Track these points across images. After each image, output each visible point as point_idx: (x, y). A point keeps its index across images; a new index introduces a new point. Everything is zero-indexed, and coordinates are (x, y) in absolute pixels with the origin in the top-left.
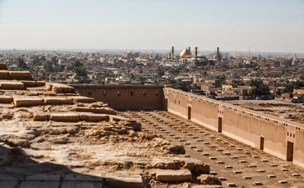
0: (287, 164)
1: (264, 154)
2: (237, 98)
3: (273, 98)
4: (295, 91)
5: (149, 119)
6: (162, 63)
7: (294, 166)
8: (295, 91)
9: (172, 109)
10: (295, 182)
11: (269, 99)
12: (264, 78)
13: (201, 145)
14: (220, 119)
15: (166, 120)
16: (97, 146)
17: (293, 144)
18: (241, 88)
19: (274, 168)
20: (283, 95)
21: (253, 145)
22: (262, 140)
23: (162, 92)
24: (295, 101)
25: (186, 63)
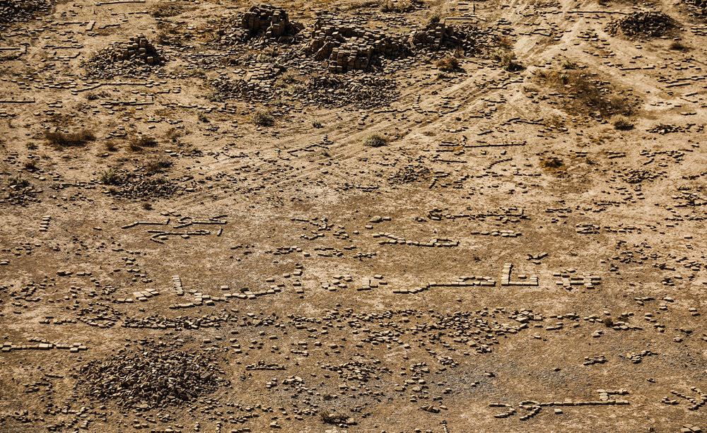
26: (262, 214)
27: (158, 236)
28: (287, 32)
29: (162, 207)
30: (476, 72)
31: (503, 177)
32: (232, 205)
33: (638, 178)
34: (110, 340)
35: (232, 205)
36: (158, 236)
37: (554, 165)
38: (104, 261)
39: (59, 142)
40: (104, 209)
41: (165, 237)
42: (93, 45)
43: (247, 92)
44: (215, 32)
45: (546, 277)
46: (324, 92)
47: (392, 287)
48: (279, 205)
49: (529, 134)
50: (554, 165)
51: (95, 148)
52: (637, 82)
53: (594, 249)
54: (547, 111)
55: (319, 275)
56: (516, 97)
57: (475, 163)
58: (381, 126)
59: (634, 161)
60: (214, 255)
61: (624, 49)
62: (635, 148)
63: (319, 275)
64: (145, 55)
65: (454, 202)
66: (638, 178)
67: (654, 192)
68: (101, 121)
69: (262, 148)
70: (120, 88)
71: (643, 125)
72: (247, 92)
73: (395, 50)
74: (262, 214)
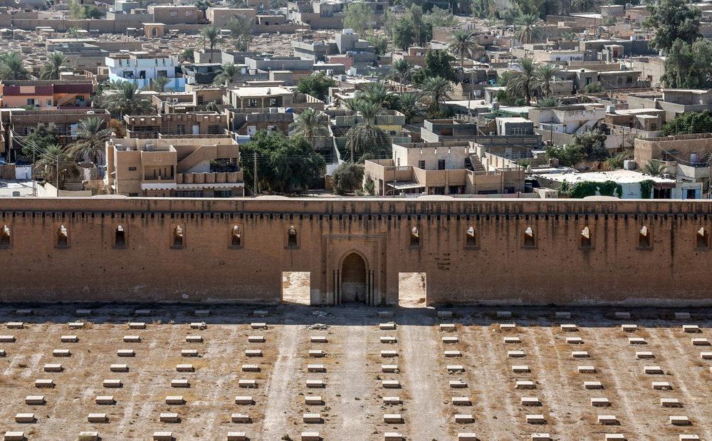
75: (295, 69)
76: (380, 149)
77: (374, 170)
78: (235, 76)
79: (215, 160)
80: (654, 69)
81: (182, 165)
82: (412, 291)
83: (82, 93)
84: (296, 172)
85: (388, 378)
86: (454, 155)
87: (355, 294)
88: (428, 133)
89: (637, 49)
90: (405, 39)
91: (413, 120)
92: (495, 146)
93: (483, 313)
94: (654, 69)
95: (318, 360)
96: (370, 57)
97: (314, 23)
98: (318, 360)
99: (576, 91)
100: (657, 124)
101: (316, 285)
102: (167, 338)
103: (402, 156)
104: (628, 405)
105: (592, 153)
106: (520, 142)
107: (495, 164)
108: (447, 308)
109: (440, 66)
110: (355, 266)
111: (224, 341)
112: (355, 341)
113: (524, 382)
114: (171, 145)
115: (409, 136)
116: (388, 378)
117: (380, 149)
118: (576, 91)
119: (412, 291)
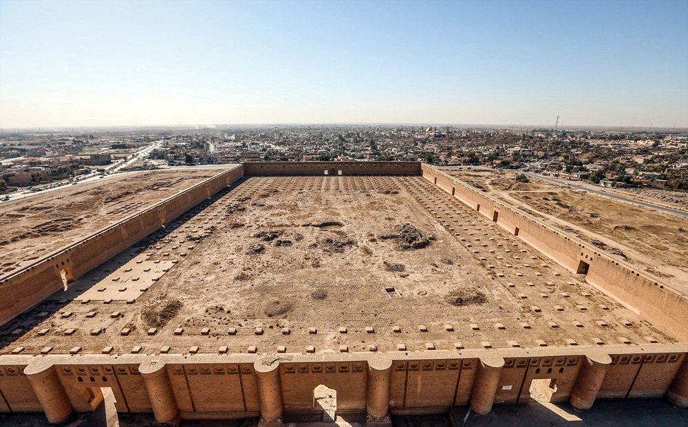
0: (493, 223)
1: (479, 214)
2: (460, 165)
3: (481, 164)
4: (494, 161)
5: (413, 183)
6: (416, 136)
7: (497, 225)
8: (494, 161)
9: (425, 176)
10: (499, 239)
11: (478, 165)
12: (588, 346)
13: (443, 205)
14: (454, 189)
15: (421, 183)
16: (400, 412)
17: (498, 213)
18: (463, 159)
19: (486, 227)
20: (487, 163)
21: (473, 207)
22: (479, 206)
23: (420, 165)
24: (494, 168)
25: (429, 136)
26: (330, 270)
27: (319, 273)
28: (331, 242)
29: (319, 269)
30: (354, 247)
31: (357, 265)
32: (327, 268)
33: (373, 264)
34: (314, 289)
35: (327, 268)
36: (319, 273)
37: (363, 262)
38: (313, 277)
39: (306, 259)
40: (312, 269)
41: (655, 209)
42: (309, 244)
43: (328, 251)
44: (323, 241)
45: (363, 279)
46: (336, 251)
47: (346, 281)
48: (532, 320)
49: (360, 257)
50: (363, 262)
51: (310, 260)
52: (372, 249)
53: (369, 275)
54: (363, 254)
55: (338, 279)
56: (358, 251)
57: (354, 262)
58: (343, 256)
59: (372, 262)
60: (325, 276)
61: (370, 243)
62: (372, 259)
63: (338, 279)
64: (315, 245)
65: (352, 268)
66: (373, 264)
67: (375, 266)
68: (311, 256)
69: (330, 259)
70: (313, 250)
71: (373, 256)
72: (328, 251)
73: (344, 244)
74: (330, 270)
75: (326, 148)
76: (336, 157)
77: (336, 159)
78: (319, 149)
79: (552, 387)
80: (369, 148)
81: (312, 159)
82: (340, 172)
83: (301, 151)
84: (327, 159)
85: (337, 182)
86: (345, 157)
87: (333, 173)
88: (342, 155)
89: (368, 146)
90: (340, 145)
91: (340, 154)
92: (350, 156)
93: (349, 175)
94: (369, 148)
95: (328, 181)
96: (334, 147)
97: (329, 144)
98: (328, 181)
99: (360, 151)
100: (370, 154)
101: (328, 172)
102: (295, 179)
103: (339, 158)
104: (365, 185)
105: (362, 157)
106: (353, 156)
107: (350, 158)
108: (344, 174)
109: (344, 147)
110: (333, 169)
111: (317, 179)
112: (333, 178)
113: (353, 182)
114: (311, 156)
115: (279, 420)
116: (337, 182)
117: (336, 157)
118: (360, 151)
119: (340, 172)
